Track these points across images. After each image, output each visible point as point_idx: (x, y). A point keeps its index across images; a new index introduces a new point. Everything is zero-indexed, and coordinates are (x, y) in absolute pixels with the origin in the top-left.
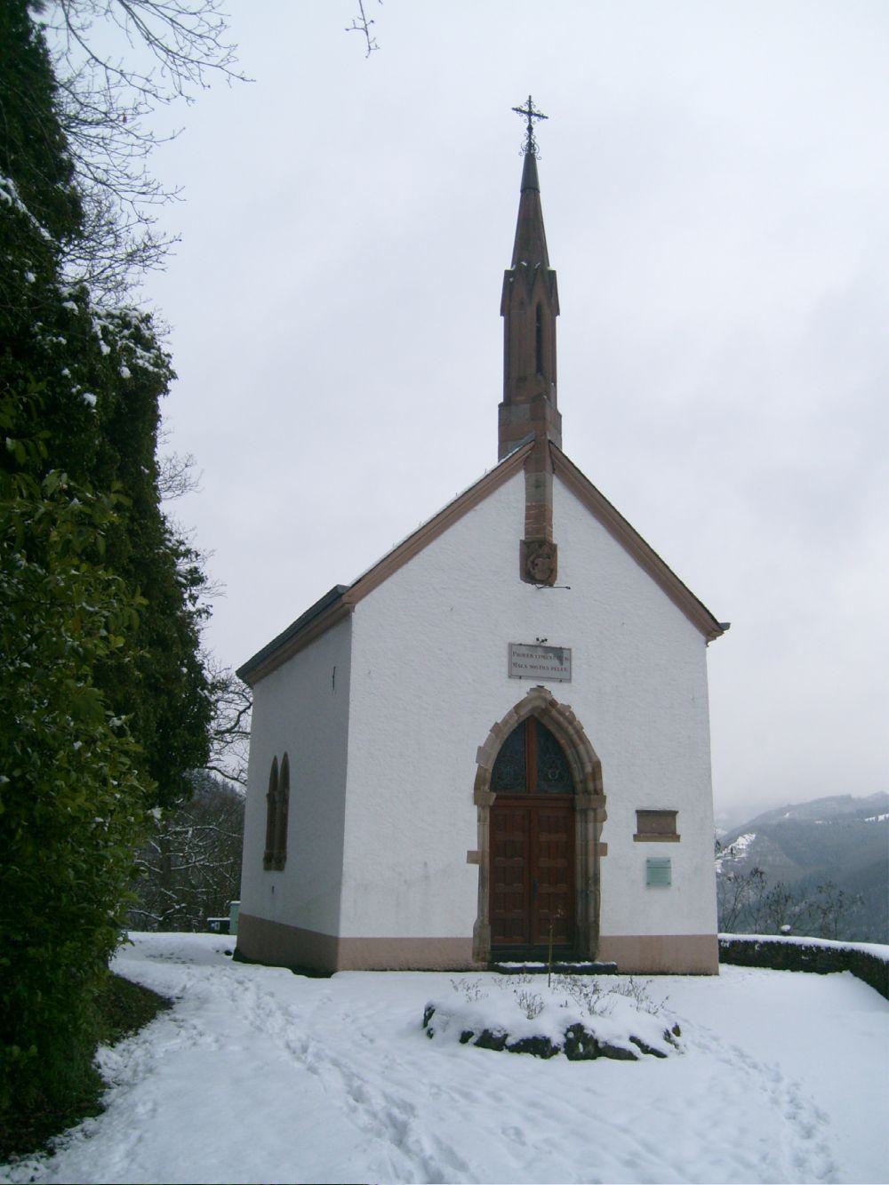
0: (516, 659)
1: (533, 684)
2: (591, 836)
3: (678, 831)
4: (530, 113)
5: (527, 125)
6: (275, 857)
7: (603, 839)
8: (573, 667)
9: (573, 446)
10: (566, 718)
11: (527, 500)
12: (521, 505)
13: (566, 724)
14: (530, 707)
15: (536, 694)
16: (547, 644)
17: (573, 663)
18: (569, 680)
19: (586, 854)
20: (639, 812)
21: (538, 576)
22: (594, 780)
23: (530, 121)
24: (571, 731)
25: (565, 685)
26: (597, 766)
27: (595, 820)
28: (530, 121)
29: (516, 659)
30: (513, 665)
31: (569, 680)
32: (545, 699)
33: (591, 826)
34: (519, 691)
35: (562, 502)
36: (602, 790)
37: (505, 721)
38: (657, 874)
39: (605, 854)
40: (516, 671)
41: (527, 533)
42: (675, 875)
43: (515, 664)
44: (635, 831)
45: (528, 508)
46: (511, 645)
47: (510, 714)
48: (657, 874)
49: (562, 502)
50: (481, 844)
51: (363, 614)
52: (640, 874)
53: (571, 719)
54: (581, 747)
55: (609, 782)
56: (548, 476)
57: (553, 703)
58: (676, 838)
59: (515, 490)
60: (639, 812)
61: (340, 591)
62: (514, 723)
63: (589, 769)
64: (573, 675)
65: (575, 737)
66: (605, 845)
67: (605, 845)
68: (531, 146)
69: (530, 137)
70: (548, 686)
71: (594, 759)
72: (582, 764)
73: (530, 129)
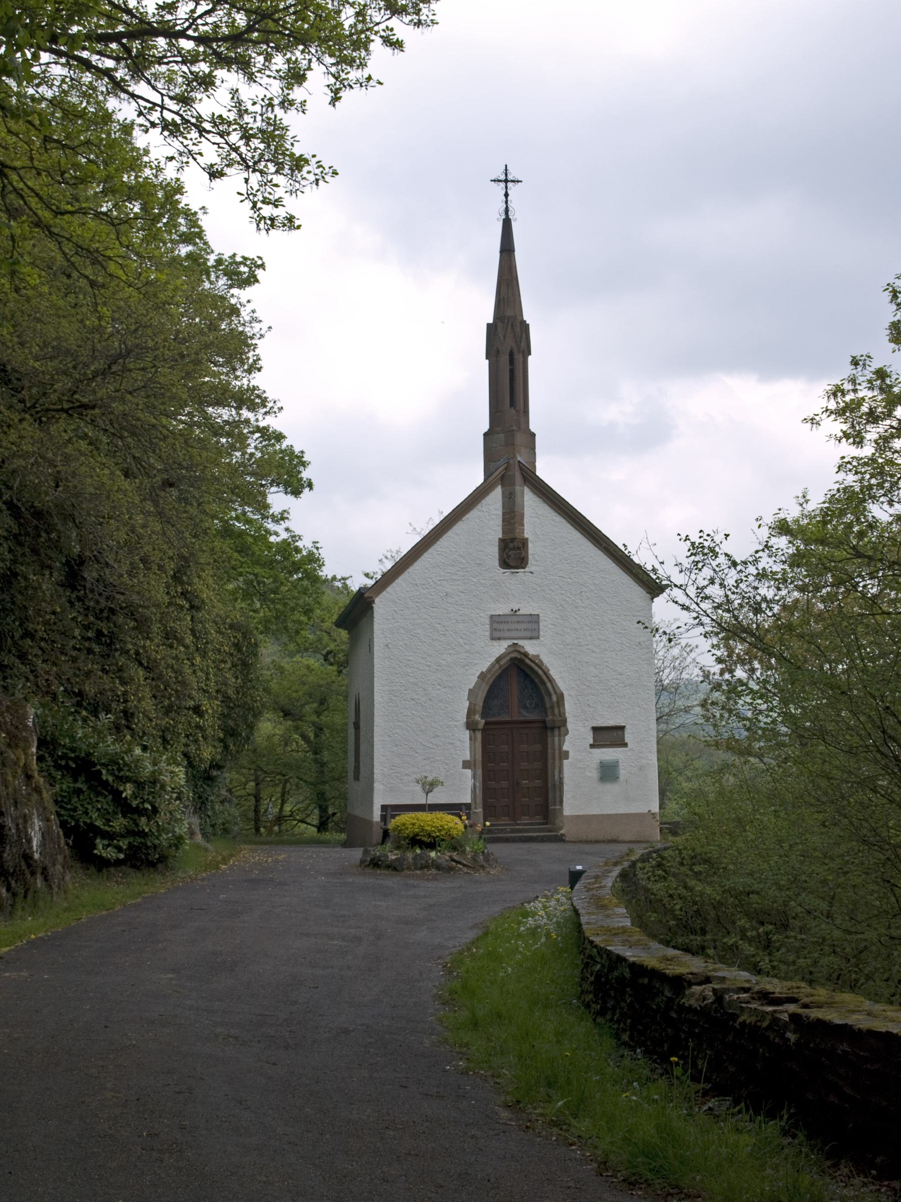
0: (495, 626)
1: (510, 642)
2: (557, 747)
3: (627, 740)
4: (506, 181)
5: (504, 192)
6: (357, 777)
7: (565, 748)
8: (541, 627)
9: (545, 470)
10: (536, 664)
11: (503, 508)
12: (498, 505)
13: (536, 668)
14: (508, 658)
15: (512, 649)
16: (521, 612)
17: (541, 624)
18: (538, 638)
19: (554, 759)
20: (595, 729)
21: (511, 564)
22: (559, 707)
23: (506, 187)
24: (540, 672)
25: (535, 641)
26: (561, 697)
27: (560, 735)
28: (506, 187)
29: (495, 626)
30: (493, 630)
31: (538, 638)
32: (519, 652)
33: (556, 739)
34: (500, 648)
35: (530, 501)
36: (564, 713)
37: (489, 670)
38: (608, 773)
39: (567, 758)
40: (497, 634)
41: (504, 532)
42: (622, 773)
43: (495, 629)
44: (591, 741)
45: (504, 514)
46: (492, 616)
47: (493, 666)
48: (608, 773)
49: (530, 501)
50: (473, 750)
51: (381, 606)
52: (593, 774)
53: (540, 665)
54: (549, 685)
55: (569, 707)
56: (518, 488)
57: (526, 655)
58: (625, 745)
59: (496, 498)
60: (595, 729)
61: (362, 591)
62: (497, 670)
63: (554, 698)
64: (541, 633)
65: (544, 677)
66: (567, 753)
67: (567, 753)
68: (507, 211)
69: (506, 202)
70: (521, 642)
71: (558, 692)
72: (550, 695)
73: (506, 195)
